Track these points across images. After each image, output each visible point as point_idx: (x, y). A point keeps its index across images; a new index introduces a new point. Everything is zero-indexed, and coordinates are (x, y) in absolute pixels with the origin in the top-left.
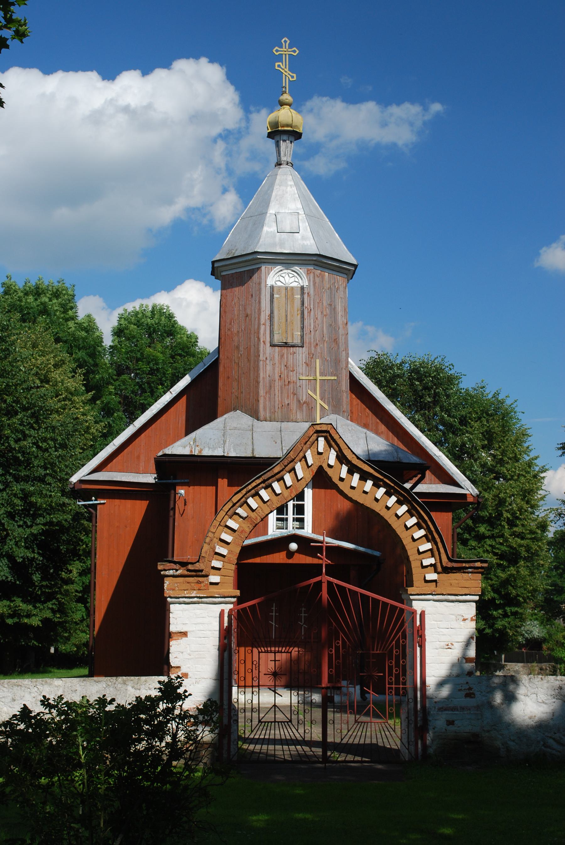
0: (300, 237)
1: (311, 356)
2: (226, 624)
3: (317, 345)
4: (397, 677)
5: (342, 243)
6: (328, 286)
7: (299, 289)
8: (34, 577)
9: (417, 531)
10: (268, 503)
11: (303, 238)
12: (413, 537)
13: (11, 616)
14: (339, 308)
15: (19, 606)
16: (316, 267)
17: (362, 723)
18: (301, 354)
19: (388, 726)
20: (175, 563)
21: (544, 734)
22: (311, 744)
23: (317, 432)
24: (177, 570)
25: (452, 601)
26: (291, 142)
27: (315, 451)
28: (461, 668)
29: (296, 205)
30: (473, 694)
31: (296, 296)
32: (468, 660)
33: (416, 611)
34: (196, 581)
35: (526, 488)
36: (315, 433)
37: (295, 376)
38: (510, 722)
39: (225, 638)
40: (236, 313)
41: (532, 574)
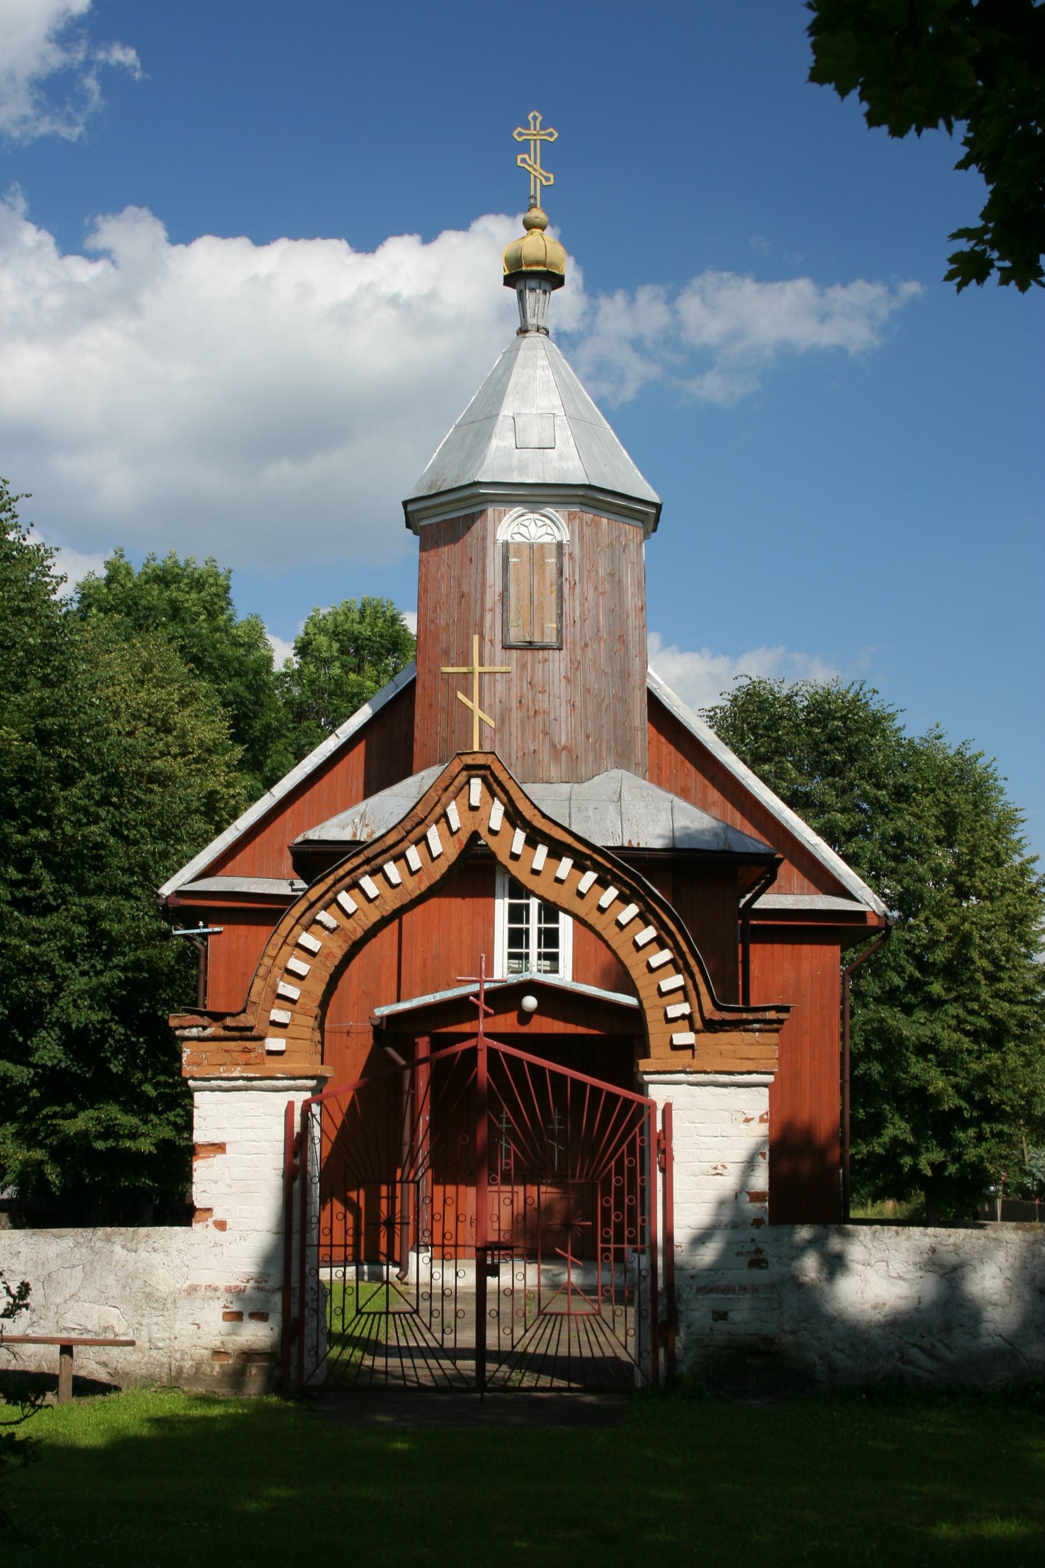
0: (555, 456)
1: (576, 665)
2: (297, 1129)
3: (586, 645)
4: (619, 1228)
5: (634, 466)
7: (554, 548)
8: (111, 1066)
9: (657, 953)
10: (377, 902)
12: (648, 965)
13: (104, 1136)
14: (629, 581)
15: (116, 1118)
16: (584, 508)
18: (558, 663)
20: (202, 1014)
21: (901, 1338)
22: (456, 1354)
23: (468, 767)
24: (205, 1028)
25: (725, 1085)
26: (545, 292)
27: (464, 805)
30: (765, 1261)
32: (756, 1197)
33: (654, 1104)
34: (240, 1049)
35: (1015, 912)
37: (547, 700)
38: (836, 1314)
39: (295, 1155)
41: (1028, 1063)
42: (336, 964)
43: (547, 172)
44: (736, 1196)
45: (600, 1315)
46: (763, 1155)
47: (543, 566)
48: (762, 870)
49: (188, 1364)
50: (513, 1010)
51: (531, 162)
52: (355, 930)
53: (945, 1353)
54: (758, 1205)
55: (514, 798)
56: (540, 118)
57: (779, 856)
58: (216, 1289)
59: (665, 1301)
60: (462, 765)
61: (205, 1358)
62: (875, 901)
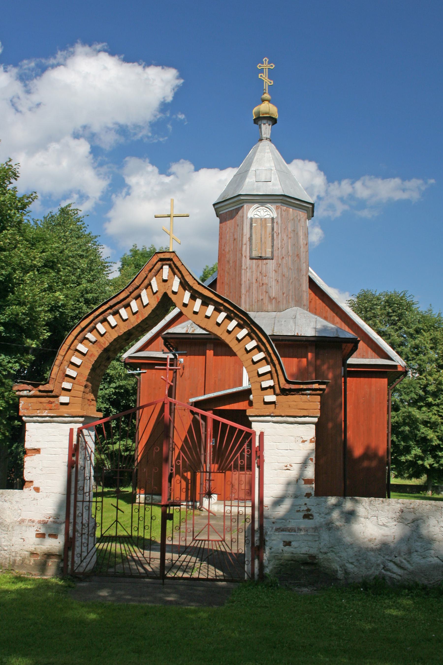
1: (279, 265)
2: (75, 442)
3: (283, 258)
6: (292, 218)
7: (270, 219)
10: (116, 328)
11: (274, 185)
16: (283, 205)
17: (200, 540)
18: (271, 264)
19: (224, 544)
21: (384, 557)
23: (161, 260)
24: (30, 391)
28: (298, 488)
29: (272, 165)
30: (311, 515)
31: (269, 225)
32: (308, 481)
33: (255, 432)
34: (47, 401)
36: (158, 261)
39: (73, 455)
40: (228, 238)
42: (95, 360)
43: (271, 80)
44: (297, 481)
45: (224, 541)
46: (312, 460)
47: (266, 227)
48: (352, 345)
49: (18, 558)
50: (246, 400)
51: (264, 77)
52: (105, 343)
53: (408, 566)
54: (309, 486)
55: (184, 275)
56: (268, 60)
57: (359, 339)
58: (33, 522)
59: (258, 535)
60: (158, 259)
61: (27, 556)
62: (401, 361)
